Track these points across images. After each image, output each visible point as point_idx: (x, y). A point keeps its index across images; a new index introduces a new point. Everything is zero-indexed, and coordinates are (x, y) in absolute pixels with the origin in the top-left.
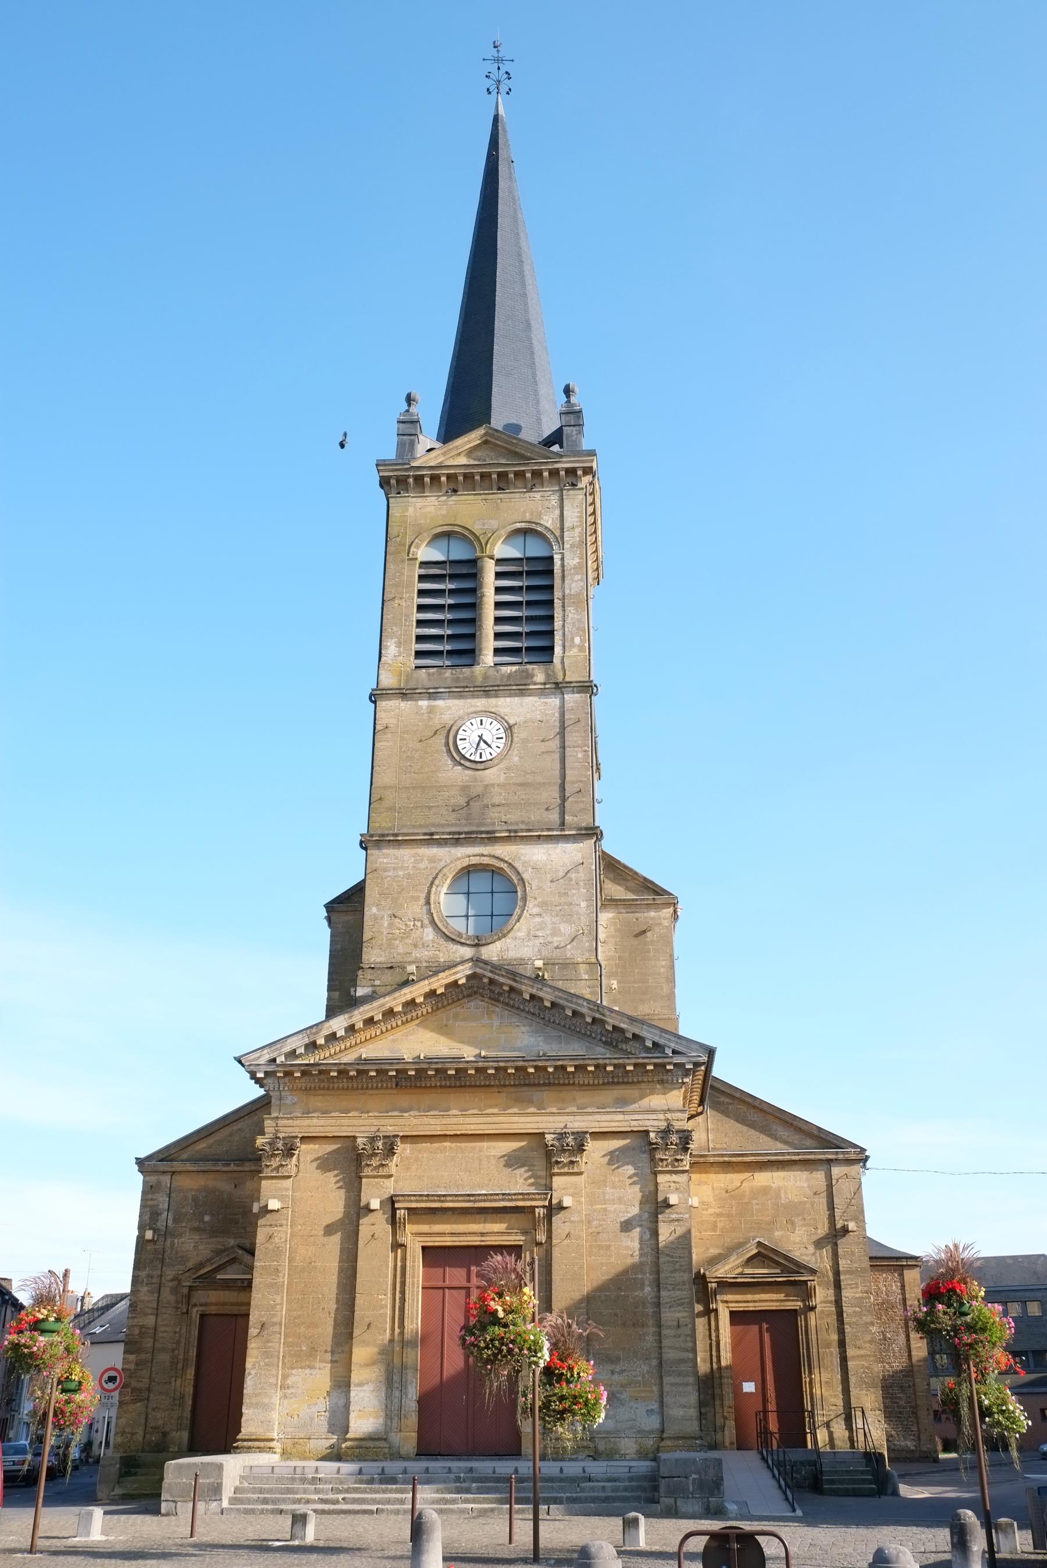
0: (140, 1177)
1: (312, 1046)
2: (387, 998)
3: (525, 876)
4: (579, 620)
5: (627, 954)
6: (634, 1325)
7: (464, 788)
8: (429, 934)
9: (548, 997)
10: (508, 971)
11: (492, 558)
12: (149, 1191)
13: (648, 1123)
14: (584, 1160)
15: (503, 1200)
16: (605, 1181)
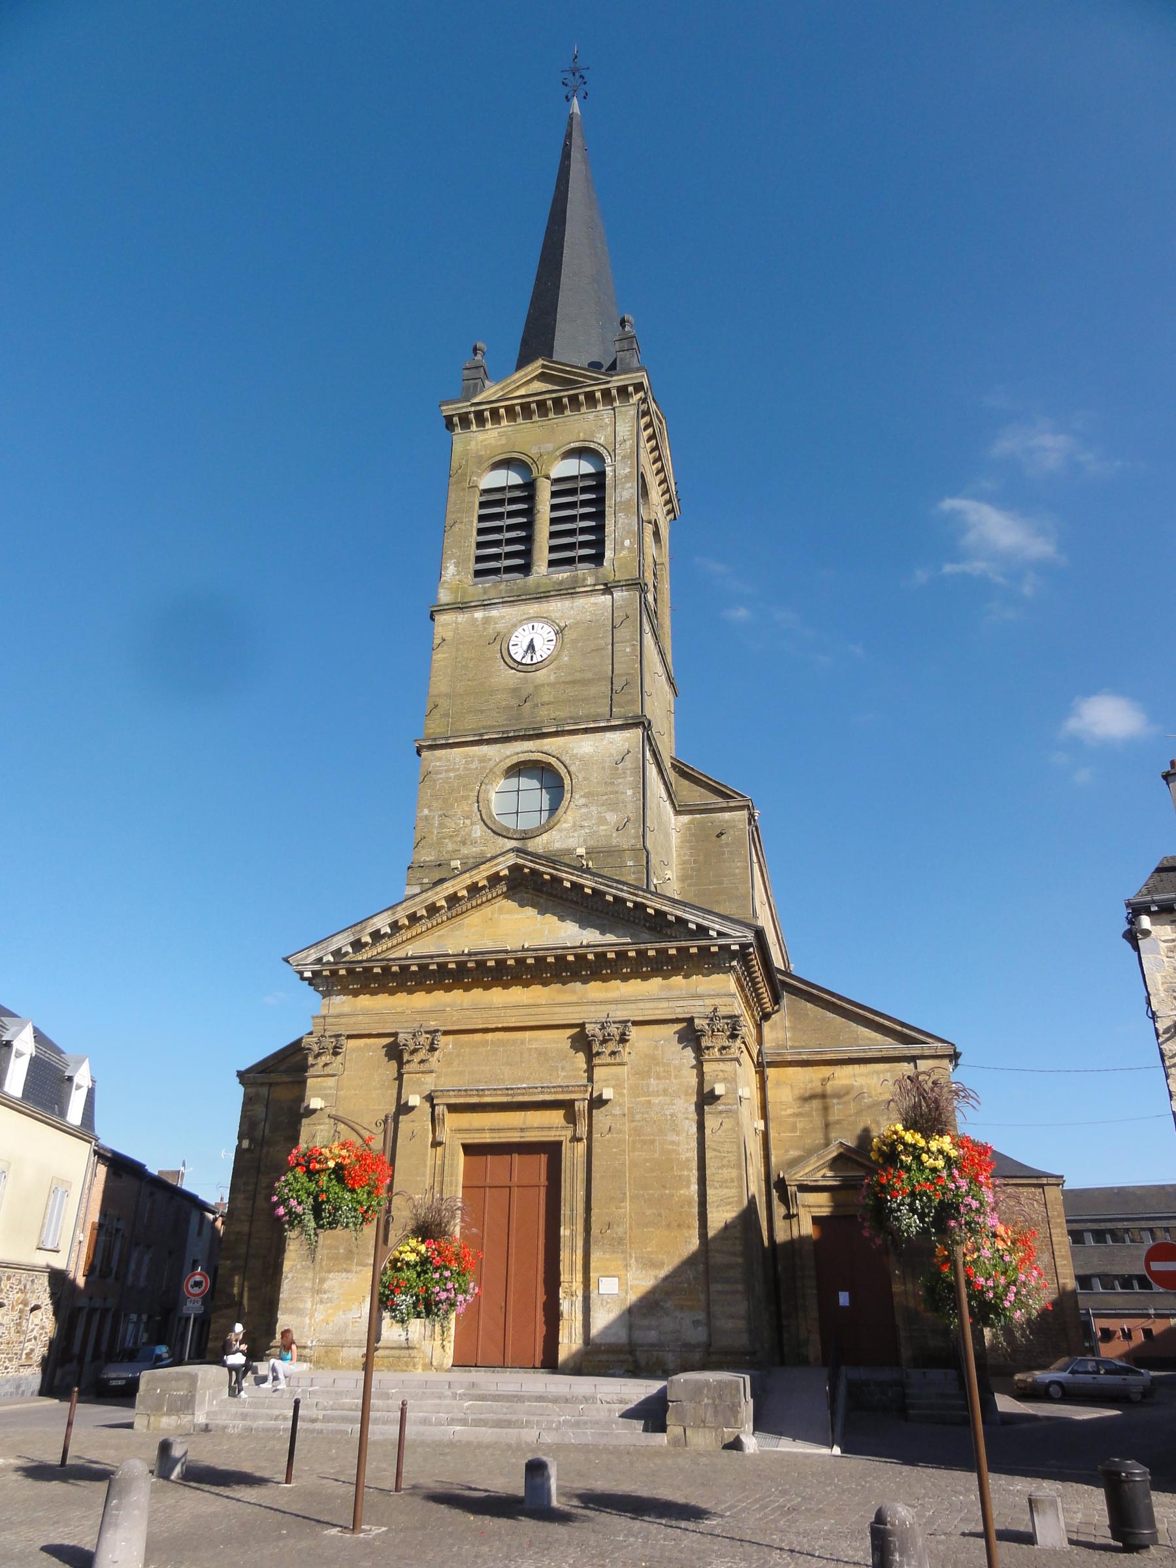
0: (241, 1090)
1: (357, 945)
2: (430, 893)
3: (572, 769)
4: (630, 524)
5: (701, 858)
6: (679, 1226)
7: (515, 691)
8: (478, 831)
9: (588, 883)
10: (547, 859)
11: (548, 478)
12: (248, 1101)
13: (693, 1009)
14: (627, 1050)
15: (542, 1093)
16: (649, 1072)
